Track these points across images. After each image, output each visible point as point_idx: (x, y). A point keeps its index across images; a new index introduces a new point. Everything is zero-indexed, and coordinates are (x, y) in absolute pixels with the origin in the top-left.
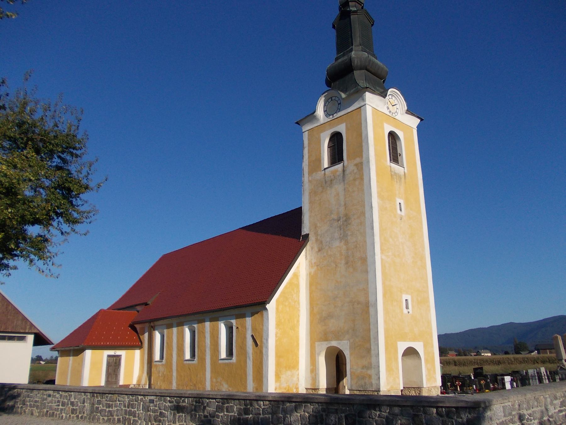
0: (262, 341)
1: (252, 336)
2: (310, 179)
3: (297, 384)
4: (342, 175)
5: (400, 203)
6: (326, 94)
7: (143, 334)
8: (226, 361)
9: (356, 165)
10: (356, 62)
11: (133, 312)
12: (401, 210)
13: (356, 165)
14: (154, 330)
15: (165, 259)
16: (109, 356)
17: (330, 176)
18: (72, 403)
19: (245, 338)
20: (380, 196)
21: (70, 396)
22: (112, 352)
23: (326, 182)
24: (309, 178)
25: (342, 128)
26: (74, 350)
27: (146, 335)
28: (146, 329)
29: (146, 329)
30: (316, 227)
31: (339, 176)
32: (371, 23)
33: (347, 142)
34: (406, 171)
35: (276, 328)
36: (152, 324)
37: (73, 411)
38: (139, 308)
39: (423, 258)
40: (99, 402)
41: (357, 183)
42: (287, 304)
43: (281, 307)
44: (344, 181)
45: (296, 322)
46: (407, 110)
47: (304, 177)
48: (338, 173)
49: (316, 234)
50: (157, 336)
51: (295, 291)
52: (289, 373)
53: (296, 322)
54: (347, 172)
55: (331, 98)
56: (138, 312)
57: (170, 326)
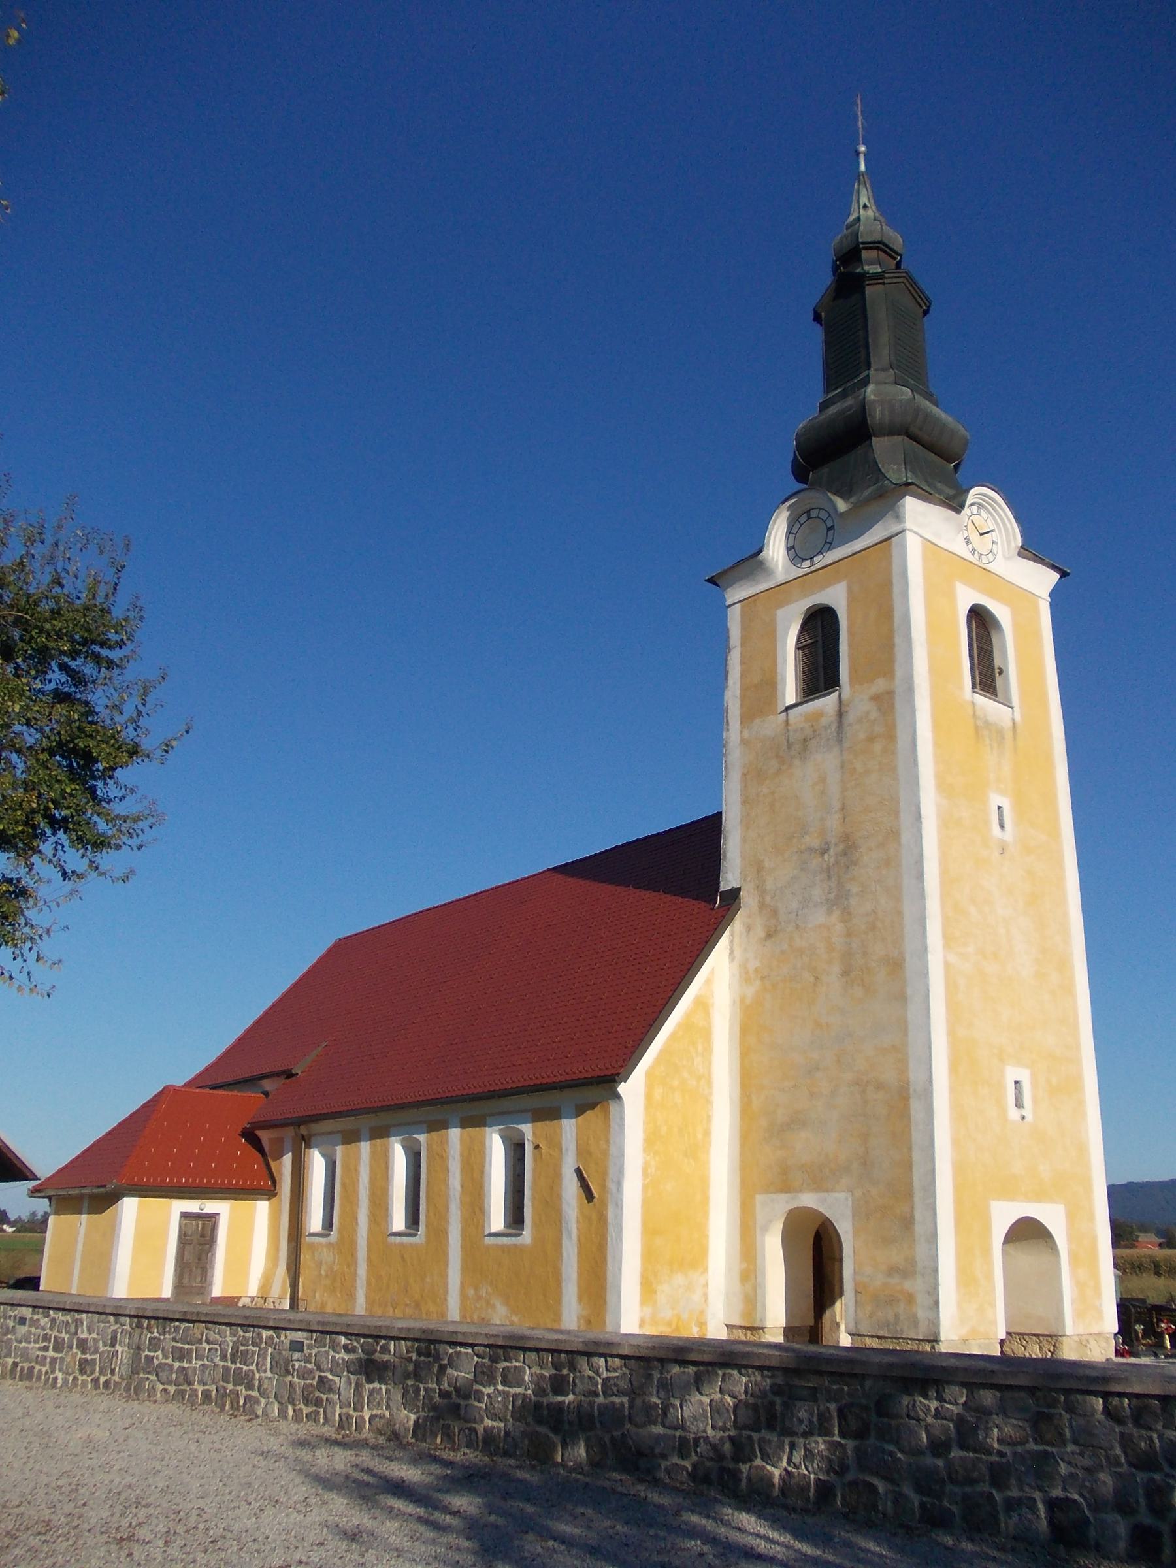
0: (603, 1187)
1: (578, 1172)
2: (746, 734)
3: (702, 1312)
4: (834, 726)
5: (999, 808)
6: (794, 500)
7: (279, 1156)
8: (505, 1240)
9: (876, 698)
10: (878, 415)
11: (254, 1095)
12: (1002, 826)
13: (876, 698)
14: (308, 1146)
15: (343, 949)
16: (185, 1216)
17: (802, 729)
18: (83, 1345)
19: (557, 1176)
20: (942, 786)
21: (78, 1323)
22: (193, 1206)
23: (790, 746)
24: (741, 732)
25: (836, 596)
26: (93, 1198)
27: (288, 1159)
28: (288, 1143)
29: (288, 1143)
30: (759, 868)
31: (826, 728)
32: (921, 307)
33: (851, 634)
34: (1018, 717)
35: (645, 1150)
36: (303, 1130)
37: (84, 1366)
38: (267, 1085)
39: (1064, 964)
40: (154, 1344)
41: (877, 747)
42: (676, 1083)
43: (658, 1092)
44: (840, 741)
45: (700, 1136)
46: (1021, 547)
47: (728, 730)
48: (824, 721)
49: (761, 890)
50: (317, 1163)
51: (700, 1048)
52: (679, 1279)
53: (700, 1136)
54: (851, 717)
55: (808, 512)
56: (266, 1094)
57: (351, 1138)
